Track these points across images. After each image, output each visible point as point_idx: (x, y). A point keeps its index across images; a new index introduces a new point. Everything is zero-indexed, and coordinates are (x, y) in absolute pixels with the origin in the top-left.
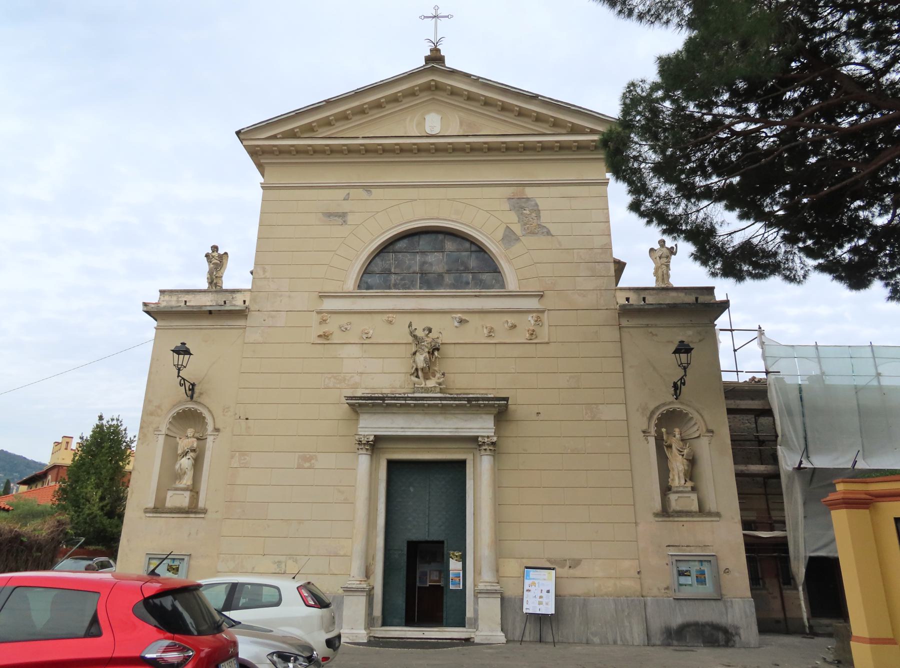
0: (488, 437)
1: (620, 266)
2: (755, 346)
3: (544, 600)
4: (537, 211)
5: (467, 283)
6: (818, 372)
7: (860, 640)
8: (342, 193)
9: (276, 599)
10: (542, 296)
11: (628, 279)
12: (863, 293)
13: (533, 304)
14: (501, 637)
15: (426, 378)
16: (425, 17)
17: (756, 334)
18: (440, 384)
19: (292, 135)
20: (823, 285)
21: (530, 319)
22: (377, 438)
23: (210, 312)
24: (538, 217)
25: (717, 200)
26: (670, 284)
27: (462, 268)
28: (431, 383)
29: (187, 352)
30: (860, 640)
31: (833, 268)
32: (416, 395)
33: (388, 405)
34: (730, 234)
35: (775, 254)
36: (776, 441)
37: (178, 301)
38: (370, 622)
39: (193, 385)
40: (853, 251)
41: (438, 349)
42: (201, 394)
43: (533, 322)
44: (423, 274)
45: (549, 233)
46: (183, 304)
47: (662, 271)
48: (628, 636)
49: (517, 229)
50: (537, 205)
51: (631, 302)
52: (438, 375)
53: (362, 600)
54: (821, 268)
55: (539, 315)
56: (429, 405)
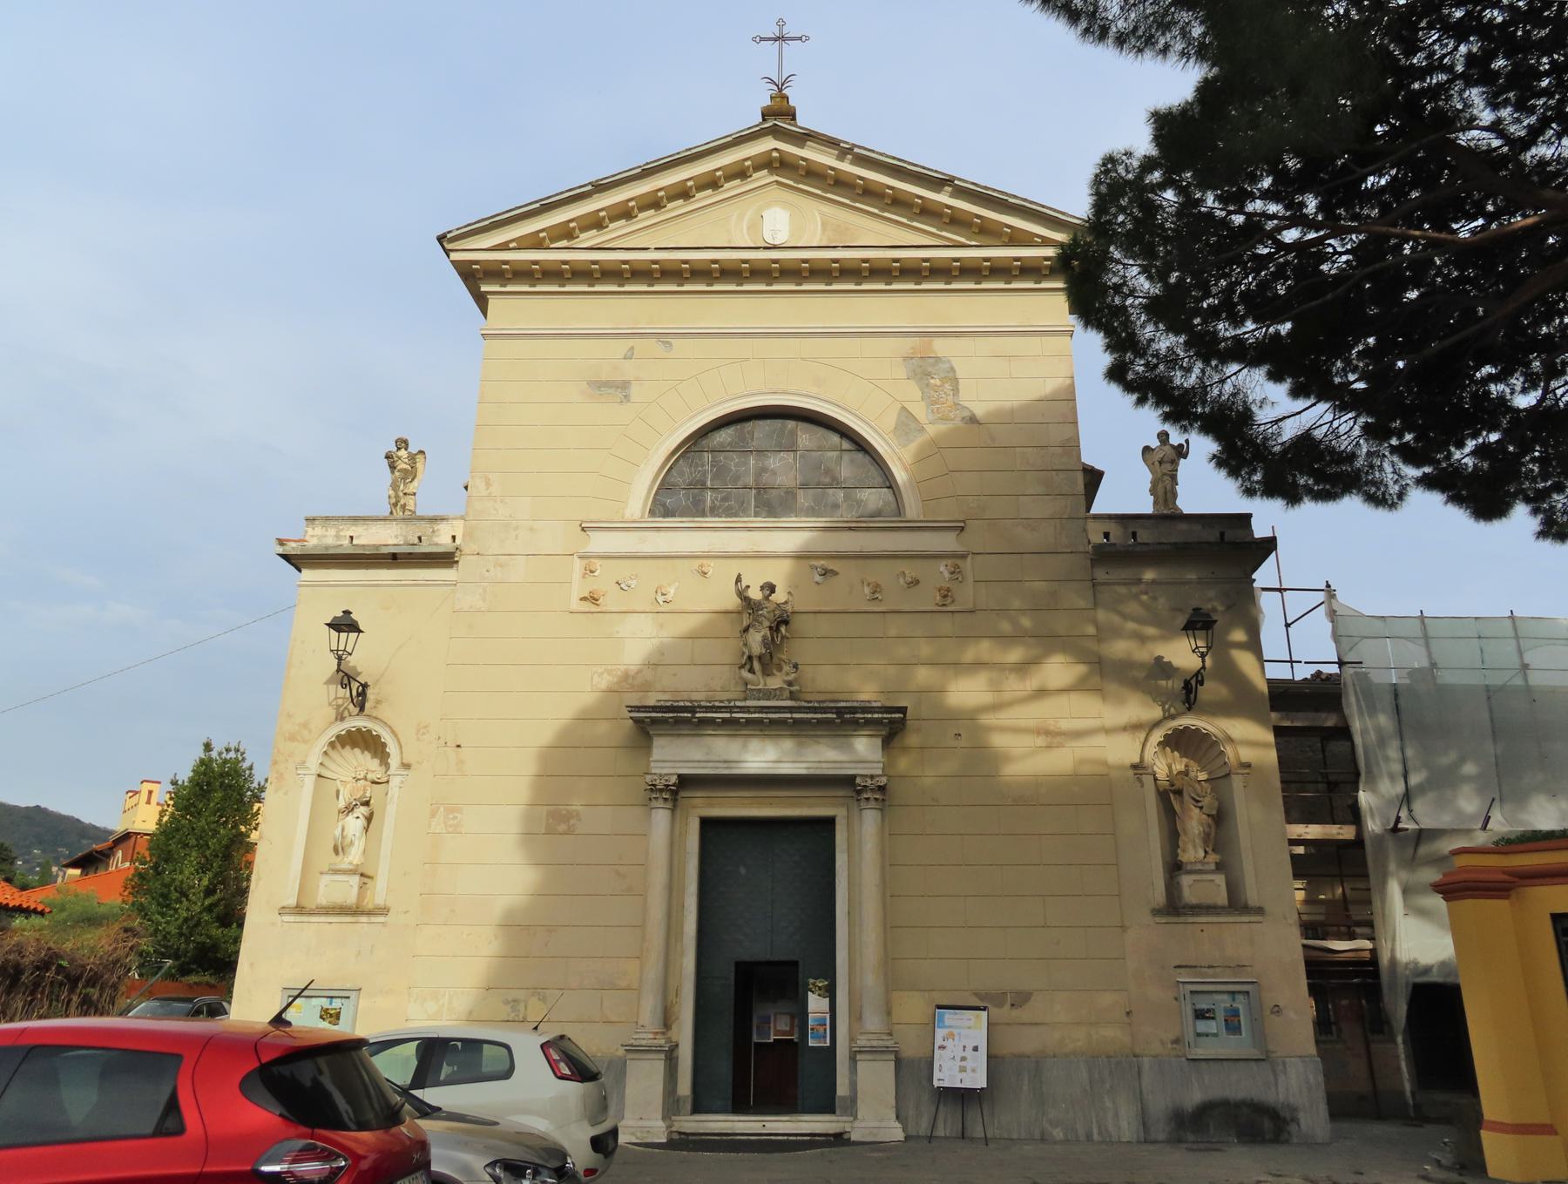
0: (872, 777)
1: (1093, 478)
8: (622, 346)
10: (962, 529)
11: (1106, 502)
14: (896, 1133)
15: (767, 672)
16: (762, 39)
18: (790, 684)
19: (534, 242)
20: (1429, 510)
21: (942, 568)
22: (686, 782)
23: (394, 556)
24: (956, 390)
27: (827, 480)
28: (775, 682)
29: (353, 627)
31: (1448, 483)
35: (1352, 457)
37: (337, 537)
38: (671, 1106)
39: (365, 686)
41: (786, 622)
42: (378, 702)
43: (947, 575)
44: (761, 489)
46: (346, 542)
47: (1165, 487)
50: (952, 369)
52: (786, 668)
53: (658, 1066)
54: (1427, 482)
55: (959, 562)
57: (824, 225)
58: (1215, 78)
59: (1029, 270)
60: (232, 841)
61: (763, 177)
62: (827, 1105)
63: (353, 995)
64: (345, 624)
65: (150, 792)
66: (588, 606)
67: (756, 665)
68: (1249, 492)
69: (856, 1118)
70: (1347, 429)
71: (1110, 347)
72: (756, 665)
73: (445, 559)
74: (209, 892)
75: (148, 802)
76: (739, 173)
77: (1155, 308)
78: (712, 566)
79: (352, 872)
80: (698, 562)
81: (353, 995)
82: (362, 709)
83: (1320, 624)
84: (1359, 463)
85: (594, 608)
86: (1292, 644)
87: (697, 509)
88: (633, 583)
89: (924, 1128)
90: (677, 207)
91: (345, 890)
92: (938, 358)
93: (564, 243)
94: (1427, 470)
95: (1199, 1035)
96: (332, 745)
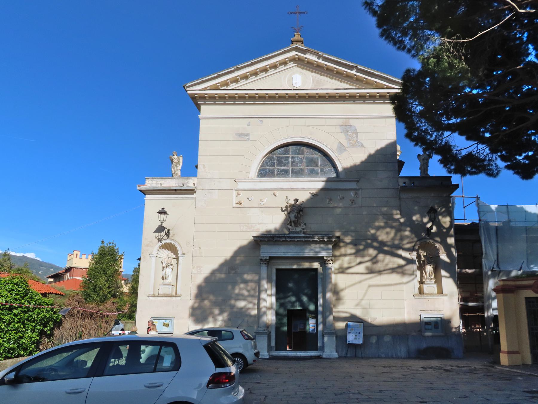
1: (401, 164)
2: (474, 205)
3: (357, 337)
4: (356, 132)
5: (317, 173)
6: (507, 219)
7: (504, 352)
8: (246, 122)
9: (232, 337)
10: (358, 181)
11: (405, 173)
12: (529, 181)
13: (353, 185)
14: (336, 355)
15: (296, 226)
17: (475, 199)
18: (303, 229)
20: (508, 176)
21: (352, 194)
22: (271, 258)
23: (175, 190)
24: (357, 137)
25: (453, 131)
26: (428, 174)
28: (299, 229)
29: (165, 213)
30: (504, 352)
31: (515, 167)
32: (291, 235)
33: (276, 241)
34: (460, 150)
35: (484, 160)
36: (482, 256)
37: (157, 184)
38: (270, 349)
39: (169, 230)
40: (527, 157)
41: (302, 211)
42: (174, 235)
43: (353, 196)
45: (362, 146)
46: (159, 186)
47: (424, 167)
48: (399, 354)
49: (345, 143)
50: (356, 130)
51: (407, 185)
52: (302, 225)
53: (266, 338)
54: (507, 167)
55: (357, 191)
56: (298, 241)
57: (313, 80)
58: (423, 110)
59: (382, 97)
60: (114, 272)
61: (292, 64)
62: (316, 349)
63: (172, 319)
64: (162, 212)
65: (77, 254)
66: (238, 205)
67: (293, 224)
68: (450, 172)
69: (324, 352)
70: (482, 150)
71: (406, 128)
72: (293, 224)
73: (191, 191)
74: (109, 288)
75: (76, 257)
76: (284, 63)
77: (422, 114)
78: (277, 193)
79: (169, 285)
80: (273, 192)
81: (172, 319)
82: (168, 237)
83: (473, 208)
84: (486, 163)
85: (240, 206)
86: (464, 214)
87: (284, 173)
88: (253, 198)
89: (344, 353)
90: (263, 75)
91: (168, 290)
92: (351, 126)
93: (225, 88)
94: (509, 163)
95: (426, 329)
96: (160, 248)
